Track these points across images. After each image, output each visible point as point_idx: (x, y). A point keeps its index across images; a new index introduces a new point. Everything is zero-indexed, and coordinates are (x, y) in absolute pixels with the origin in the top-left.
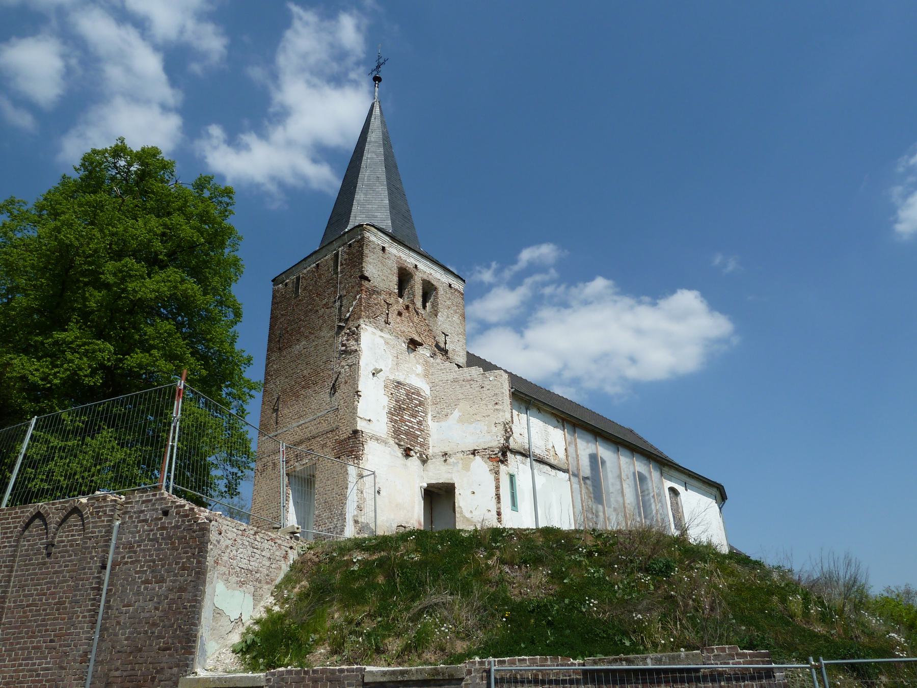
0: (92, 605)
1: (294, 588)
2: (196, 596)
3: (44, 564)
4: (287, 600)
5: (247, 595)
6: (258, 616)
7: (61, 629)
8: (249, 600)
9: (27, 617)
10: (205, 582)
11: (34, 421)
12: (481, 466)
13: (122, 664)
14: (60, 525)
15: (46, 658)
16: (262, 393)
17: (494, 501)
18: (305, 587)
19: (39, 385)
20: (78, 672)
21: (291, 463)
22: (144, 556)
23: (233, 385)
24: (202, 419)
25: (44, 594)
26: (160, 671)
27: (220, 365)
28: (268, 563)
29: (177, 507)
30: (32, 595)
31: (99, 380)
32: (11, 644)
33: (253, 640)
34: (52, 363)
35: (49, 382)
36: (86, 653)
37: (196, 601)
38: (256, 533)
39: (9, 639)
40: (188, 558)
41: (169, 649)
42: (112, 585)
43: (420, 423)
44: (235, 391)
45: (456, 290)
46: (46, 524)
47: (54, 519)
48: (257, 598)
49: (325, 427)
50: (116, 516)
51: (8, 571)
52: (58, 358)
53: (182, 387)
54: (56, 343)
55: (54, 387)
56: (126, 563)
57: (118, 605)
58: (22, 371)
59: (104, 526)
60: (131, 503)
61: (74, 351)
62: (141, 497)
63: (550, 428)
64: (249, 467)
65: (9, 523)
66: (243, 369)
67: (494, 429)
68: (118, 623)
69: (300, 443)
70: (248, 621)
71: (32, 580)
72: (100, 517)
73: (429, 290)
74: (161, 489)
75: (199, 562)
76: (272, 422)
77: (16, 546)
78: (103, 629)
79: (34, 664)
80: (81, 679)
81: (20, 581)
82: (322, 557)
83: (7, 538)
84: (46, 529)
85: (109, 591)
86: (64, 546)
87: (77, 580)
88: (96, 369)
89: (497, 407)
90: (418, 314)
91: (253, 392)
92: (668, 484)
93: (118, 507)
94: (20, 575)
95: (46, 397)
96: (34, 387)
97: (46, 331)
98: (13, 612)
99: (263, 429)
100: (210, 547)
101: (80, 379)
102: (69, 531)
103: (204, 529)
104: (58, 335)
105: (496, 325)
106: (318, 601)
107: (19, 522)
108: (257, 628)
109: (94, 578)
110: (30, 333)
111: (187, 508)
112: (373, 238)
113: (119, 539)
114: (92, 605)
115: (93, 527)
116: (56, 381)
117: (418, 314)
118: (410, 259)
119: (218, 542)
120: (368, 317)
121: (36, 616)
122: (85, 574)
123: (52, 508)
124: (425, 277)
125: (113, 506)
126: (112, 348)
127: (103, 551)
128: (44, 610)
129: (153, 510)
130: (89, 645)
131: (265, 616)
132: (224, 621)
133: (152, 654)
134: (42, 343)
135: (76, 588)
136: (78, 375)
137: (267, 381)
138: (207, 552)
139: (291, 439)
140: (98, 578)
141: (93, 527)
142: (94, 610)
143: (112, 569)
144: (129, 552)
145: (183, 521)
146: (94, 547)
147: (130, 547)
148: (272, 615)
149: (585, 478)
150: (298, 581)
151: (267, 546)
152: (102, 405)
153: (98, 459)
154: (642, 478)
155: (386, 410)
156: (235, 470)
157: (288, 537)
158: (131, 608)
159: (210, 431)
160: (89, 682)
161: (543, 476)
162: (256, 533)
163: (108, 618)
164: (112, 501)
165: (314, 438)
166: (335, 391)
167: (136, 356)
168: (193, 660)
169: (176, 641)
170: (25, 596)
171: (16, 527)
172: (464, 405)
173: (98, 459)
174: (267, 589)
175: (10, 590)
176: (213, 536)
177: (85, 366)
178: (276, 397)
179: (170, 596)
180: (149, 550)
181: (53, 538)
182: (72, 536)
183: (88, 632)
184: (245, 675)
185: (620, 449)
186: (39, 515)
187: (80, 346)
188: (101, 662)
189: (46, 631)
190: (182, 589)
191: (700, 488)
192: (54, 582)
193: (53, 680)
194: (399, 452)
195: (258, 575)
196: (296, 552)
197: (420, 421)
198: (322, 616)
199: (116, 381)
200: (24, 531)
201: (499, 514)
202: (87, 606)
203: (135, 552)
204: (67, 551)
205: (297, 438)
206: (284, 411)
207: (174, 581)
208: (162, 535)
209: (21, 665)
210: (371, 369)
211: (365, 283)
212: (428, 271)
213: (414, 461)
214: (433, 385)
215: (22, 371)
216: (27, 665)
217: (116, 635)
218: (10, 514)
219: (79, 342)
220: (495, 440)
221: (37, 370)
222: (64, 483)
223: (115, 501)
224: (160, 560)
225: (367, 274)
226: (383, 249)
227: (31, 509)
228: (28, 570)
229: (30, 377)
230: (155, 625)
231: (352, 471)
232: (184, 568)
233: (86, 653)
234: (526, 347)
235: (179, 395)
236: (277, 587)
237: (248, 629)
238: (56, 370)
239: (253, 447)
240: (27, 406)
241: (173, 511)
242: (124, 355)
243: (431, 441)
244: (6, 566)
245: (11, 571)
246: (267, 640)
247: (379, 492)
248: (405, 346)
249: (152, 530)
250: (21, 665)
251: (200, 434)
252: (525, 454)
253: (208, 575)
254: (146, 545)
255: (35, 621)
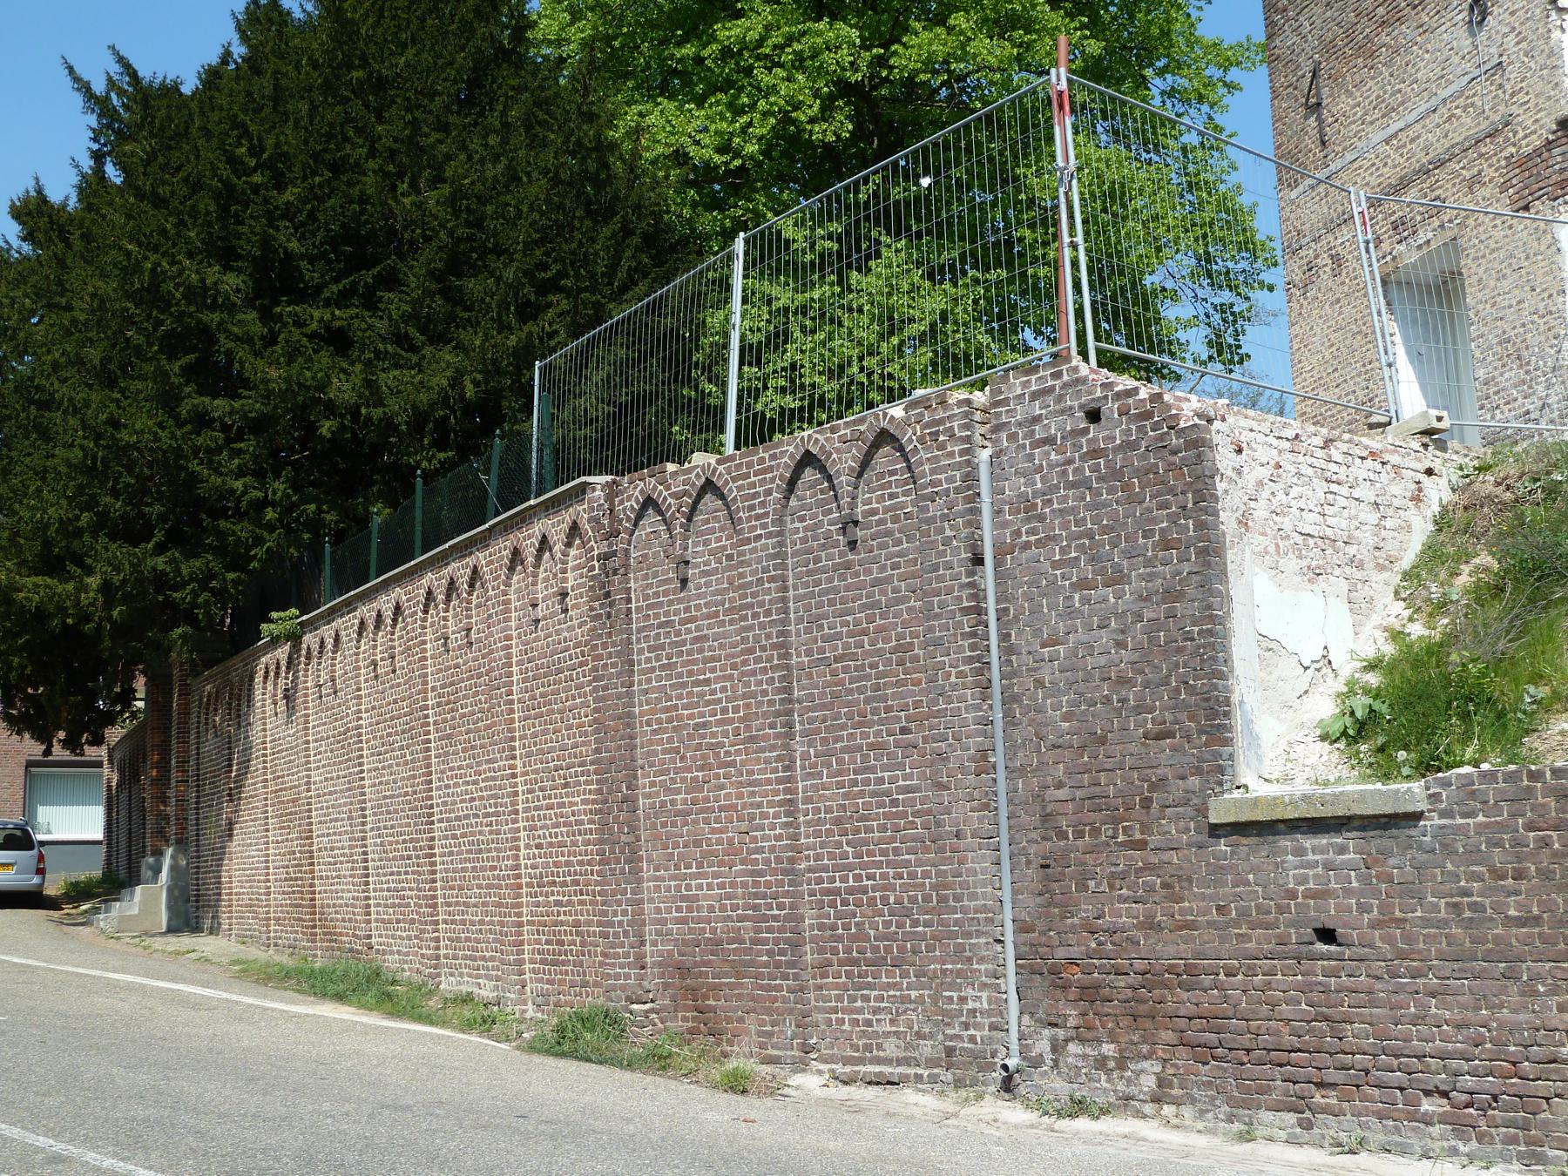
0: (973, 647)
1: (1455, 574)
2: (1210, 607)
3: (848, 566)
4: (1442, 606)
5: (1332, 600)
6: (1370, 652)
7: (917, 704)
8: (1340, 609)
9: (841, 683)
10: (1224, 572)
11: (739, 245)
13: (1069, 773)
14: (860, 475)
15: (902, 766)
16: (1263, 70)
18: (1486, 569)
19: (717, 167)
20: (976, 794)
21: (1385, 246)
22: (1065, 526)
23: (1175, 66)
24: (1112, 175)
25: (865, 633)
26: (1160, 784)
27: (1132, 17)
28: (1373, 518)
29: (1118, 396)
30: (838, 636)
31: (842, 125)
32: (824, 741)
33: (1372, 711)
34: (730, 105)
35: (737, 155)
36: (983, 754)
37: (1212, 619)
38: (1328, 443)
39: (817, 731)
40: (1173, 519)
41: (1171, 735)
42: (1007, 600)
44: (1184, 82)
46: (829, 478)
47: (844, 462)
48: (1358, 606)
49: (1468, 126)
50: (978, 439)
51: (778, 590)
52: (741, 89)
53: (1064, 85)
54: (726, 53)
55: (749, 164)
56: (1026, 546)
57: (1028, 644)
58: (673, 139)
59: (959, 466)
60: (1005, 402)
61: (772, 64)
62: (1026, 384)
64: (1262, 284)
65: (753, 485)
66: (1194, 14)
68: (1039, 683)
69: (1402, 185)
70: (1347, 668)
71: (831, 603)
72: (942, 447)
74: (1068, 359)
75: (1201, 526)
76: (1311, 142)
77: (780, 533)
78: (1009, 699)
79: (881, 781)
80: (986, 807)
81: (808, 609)
82: (1522, 488)
83: (758, 517)
84: (832, 487)
85: (1002, 613)
86: (881, 522)
87: (926, 594)
88: (831, 98)
91: (1234, 75)
93: (978, 416)
94: (804, 596)
95: (735, 190)
96: (707, 172)
97: (695, 25)
98: (810, 676)
99: (1289, 168)
100: (1221, 486)
101: (801, 131)
102: (882, 487)
103: (1197, 443)
104: (729, 32)
106: (1532, 600)
107: (772, 480)
108: (1373, 679)
109: (962, 586)
110: (664, 42)
111: (1143, 394)
113: (997, 491)
114: (973, 647)
115: (933, 472)
116: (752, 148)
119: (1239, 472)
121: (860, 679)
122: (940, 579)
123: (835, 440)
125: (966, 415)
126: (855, 33)
127: (969, 524)
128: (873, 666)
129: (1062, 412)
130: (985, 734)
131: (1389, 650)
132: (1287, 668)
133: (1133, 748)
134: (699, 60)
135: (928, 613)
136: (794, 122)
137: (1272, 29)
138: (1217, 499)
139: (1373, 181)
140: (972, 585)
141: (933, 472)
142: (979, 659)
143: (998, 563)
144: (1028, 520)
145: (1141, 429)
146: (945, 518)
147: (1026, 507)
148: (1410, 646)
150: (1465, 556)
151: (1363, 474)
152: (868, 183)
153: (891, 324)
156: (1226, 296)
157: (1416, 445)
158: (1061, 648)
159: (1139, 203)
160: (1003, 814)
162: (1328, 443)
163: (1014, 674)
164: (960, 403)
165: (1441, 164)
166: (1484, 15)
167: (915, 41)
168: (1231, 757)
169: (1183, 716)
170: (825, 639)
171: (769, 493)
173: (891, 324)
174: (1382, 585)
175: (792, 628)
176: (1224, 459)
177: (805, 97)
178: (1307, 68)
179: (1147, 615)
180: (1074, 510)
181: (853, 506)
182: (892, 496)
183: (978, 708)
184: (1370, 787)
186: (808, 459)
187: (781, 47)
188: (1022, 771)
189: (888, 709)
190: (1172, 595)
192: (875, 605)
193: (929, 812)
195: (1352, 550)
196: (1443, 482)
198: (1551, 639)
199: (886, 116)
200: (787, 498)
202: (960, 649)
203: (1041, 518)
204: (889, 533)
205: (1390, 175)
206: (1339, 104)
207: (1150, 578)
208: (1096, 469)
209: (854, 783)
215: (673, 139)
216: (867, 782)
217: (1040, 710)
218: (750, 465)
219: (776, 38)
221: (705, 130)
222: (829, 388)
223: (968, 402)
224: (1105, 530)
227: (788, 447)
228: (818, 583)
229: (692, 151)
230: (1123, 681)
232: (1166, 545)
233: (983, 754)
235: (1061, 107)
236: (1406, 576)
237: (1351, 683)
238: (744, 119)
239: (1266, 225)
240: (708, 221)
241: (1111, 408)
242: (886, 46)
244: (772, 579)
245: (785, 589)
246: (1408, 706)
249: (1070, 462)
250: (854, 783)
251: (1115, 215)
253: (1230, 555)
254: (1065, 499)
255: (861, 691)
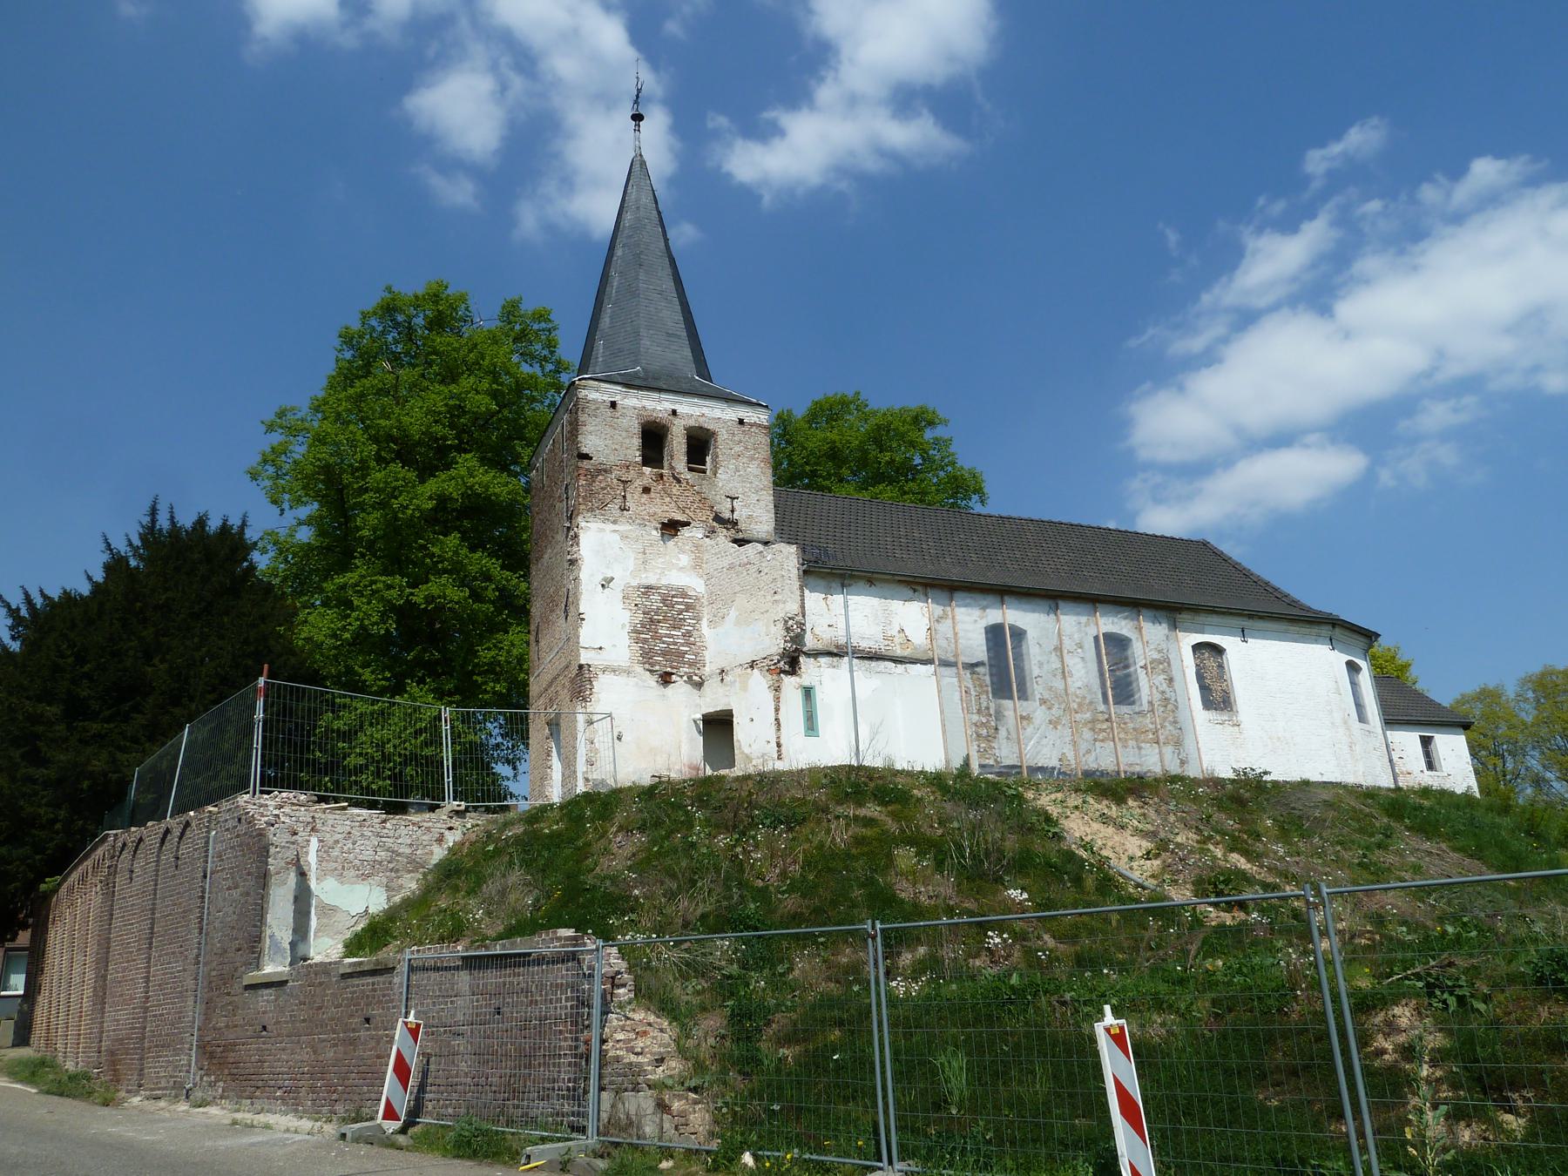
12: (759, 682)
17: (774, 728)
43: (688, 634)
45: (752, 425)
63: (896, 605)
67: (773, 629)
73: (700, 445)
89: (777, 597)
90: (679, 481)
92: (1189, 639)
105: (1275, 308)
112: (593, 395)
116: (347, 635)
117: (679, 481)
118: (658, 405)
120: (591, 510)
124: (692, 423)
149: (972, 667)
154: (1117, 644)
155: (628, 628)
161: (870, 679)
172: (741, 600)
185: (1061, 604)
191: (1286, 632)
194: (652, 681)
197: (689, 632)
201: (779, 745)
210: (599, 578)
211: (585, 464)
212: (696, 411)
213: (680, 689)
214: (708, 578)
220: (773, 643)
225: (585, 450)
226: (613, 405)
231: (581, 718)
234: (1347, 335)
243: (708, 656)
247: (619, 738)
248: (656, 534)
252: (835, 653)
